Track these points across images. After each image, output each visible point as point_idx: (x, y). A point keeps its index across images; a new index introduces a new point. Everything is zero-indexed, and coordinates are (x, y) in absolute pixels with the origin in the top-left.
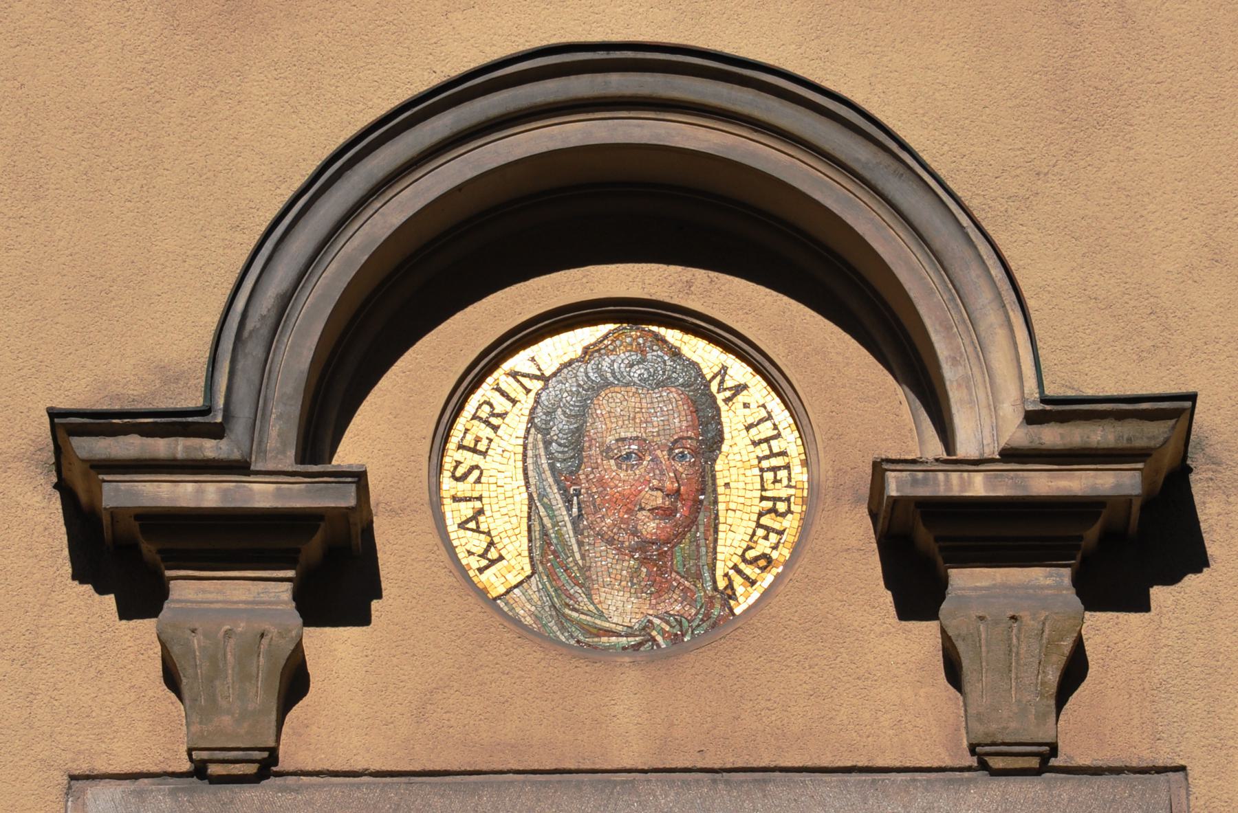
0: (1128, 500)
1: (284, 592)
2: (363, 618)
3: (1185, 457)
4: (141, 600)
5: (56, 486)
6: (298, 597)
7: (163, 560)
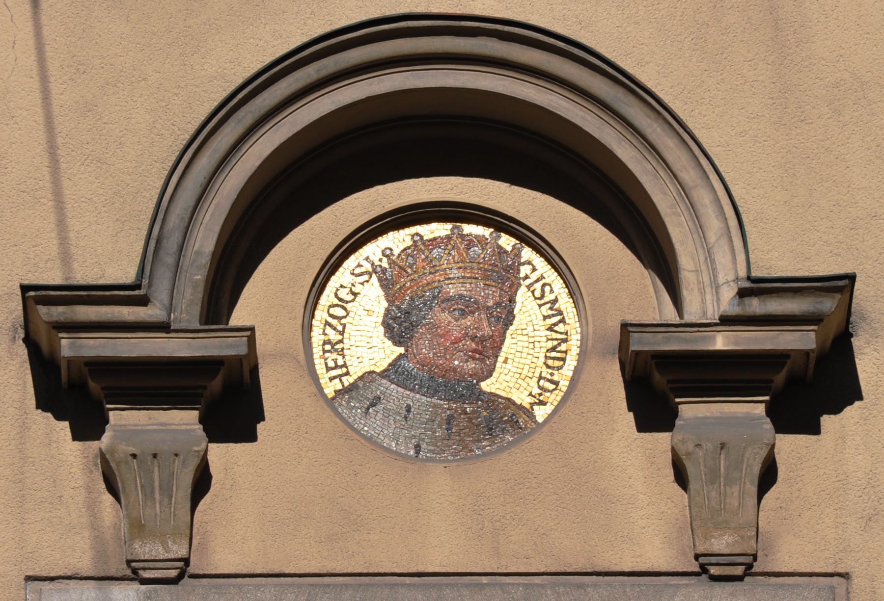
0: (807, 353)
1: (760, 409)
2: (251, 437)
3: (848, 322)
4: (88, 426)
7: (107, 396)
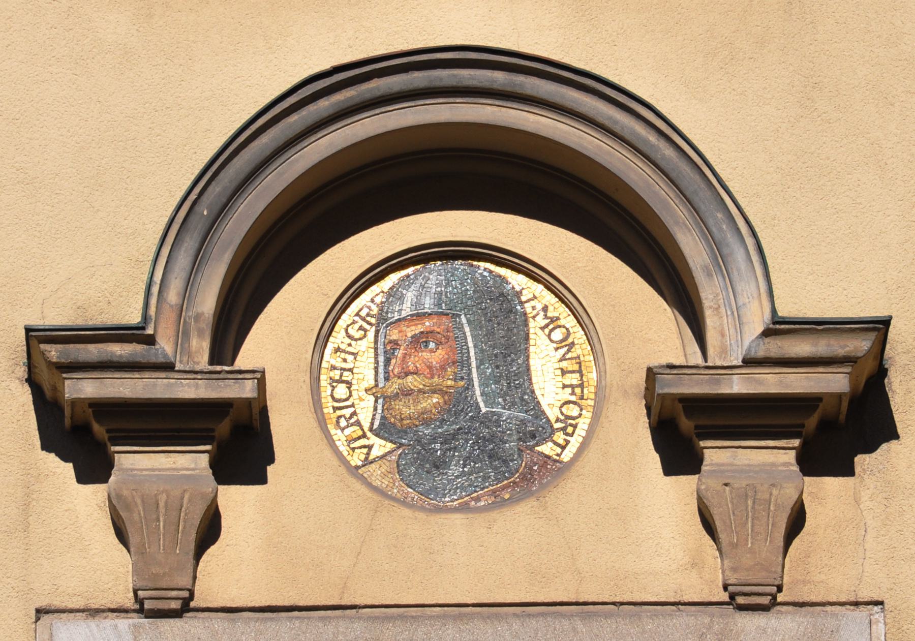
0: (840, 396)
1: (203, 460)
2: (262, 480)
4: (93, 467)
5: (27, 380)
6: (213, 465)
